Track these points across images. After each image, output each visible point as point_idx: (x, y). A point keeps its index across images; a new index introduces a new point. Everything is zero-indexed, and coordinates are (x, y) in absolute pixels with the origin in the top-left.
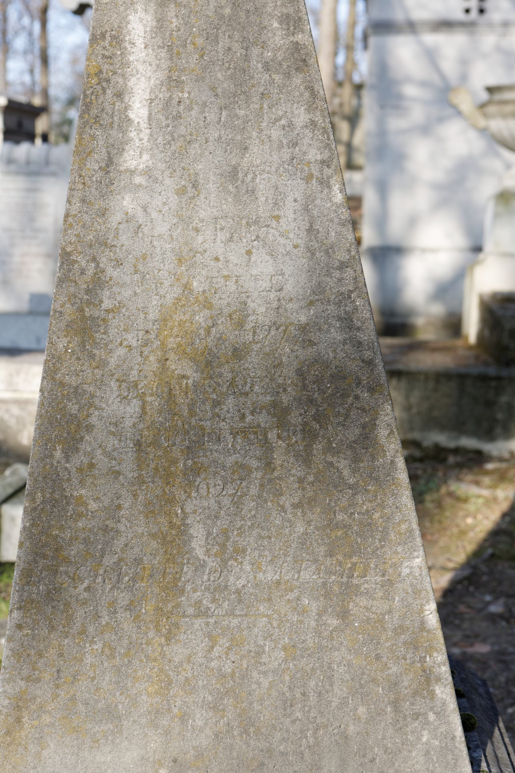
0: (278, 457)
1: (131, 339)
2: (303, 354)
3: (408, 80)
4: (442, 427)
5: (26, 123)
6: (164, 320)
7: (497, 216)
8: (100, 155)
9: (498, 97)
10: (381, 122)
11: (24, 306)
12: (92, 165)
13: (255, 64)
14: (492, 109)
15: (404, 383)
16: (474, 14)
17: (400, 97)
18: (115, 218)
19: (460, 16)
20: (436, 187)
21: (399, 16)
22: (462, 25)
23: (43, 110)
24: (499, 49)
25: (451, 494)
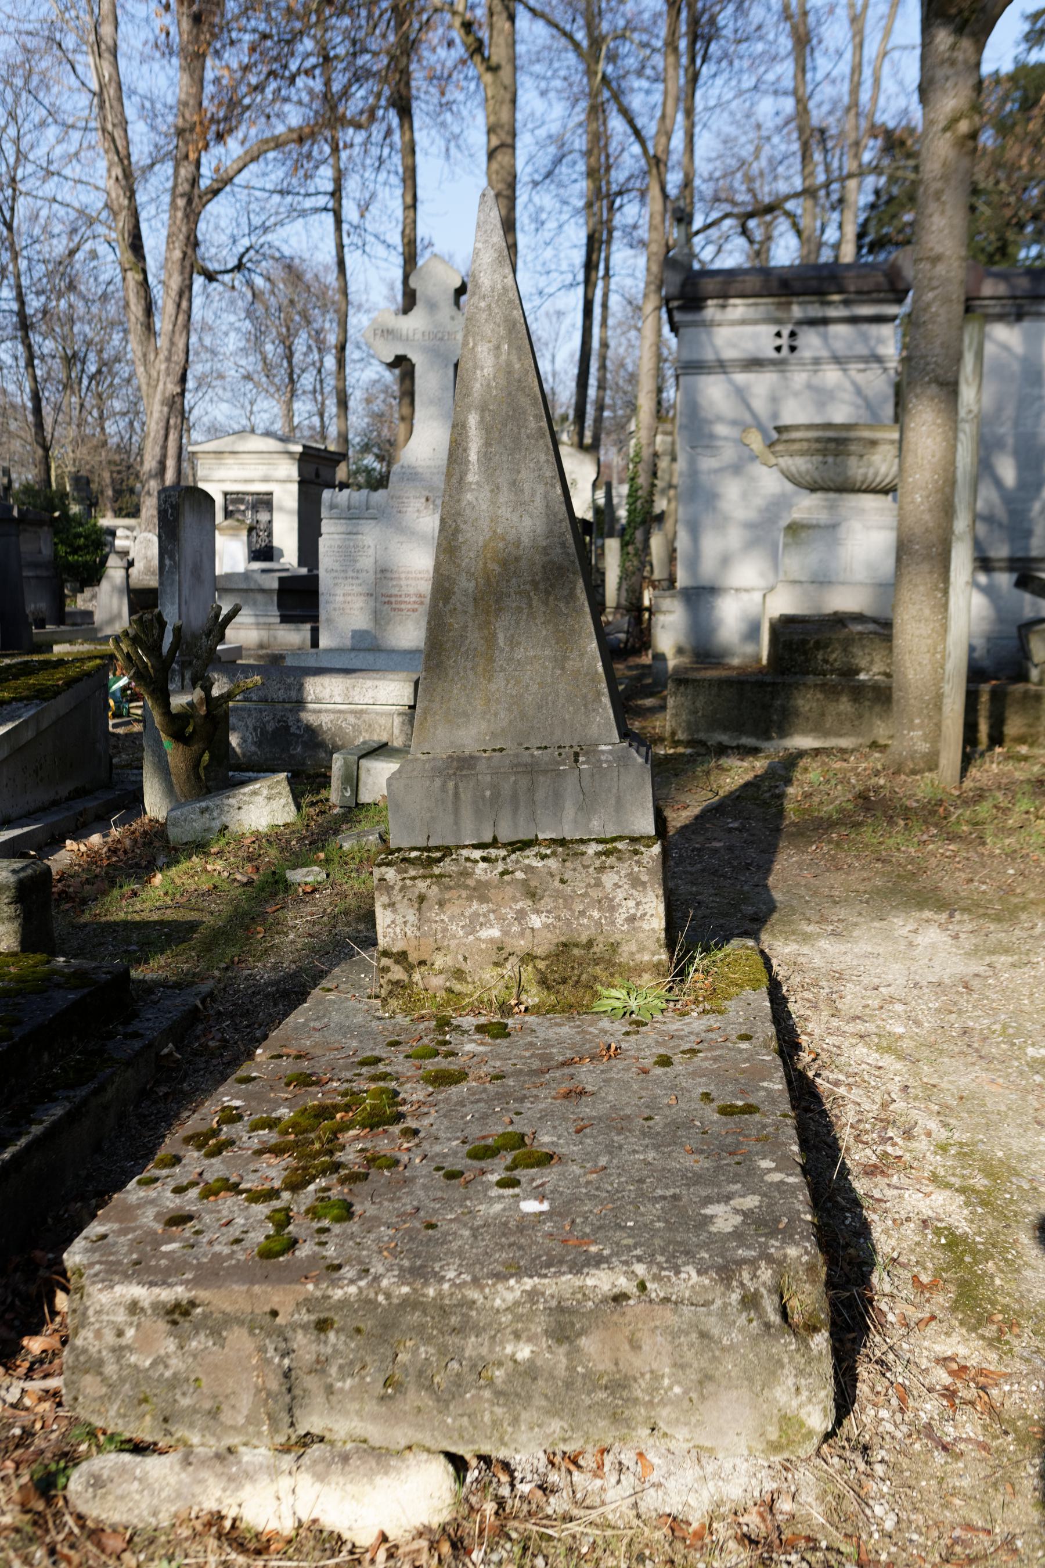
0: (535, 603)
1: (472, 555)
2: (546, 559)
3: (719, 419)
4: (725, 729)
5: (324, 472)
6: (485, 546)
7: (786, 545)
8: (456, 477)
9: (785, 436)
10: (692, 463)
11: (348, 643)
12: (454, 480)
13: (523, 436)
14: (779, 448)
15: (690, 691)
16: (785, 351)
17: (712, 436)
18: (464, 503)
19: (774, 354)
20: (749, 526)
21: (709, 355)
22: (773, 362)
23: (343, 456)
24: (809, 386)
25: (719, 767)
